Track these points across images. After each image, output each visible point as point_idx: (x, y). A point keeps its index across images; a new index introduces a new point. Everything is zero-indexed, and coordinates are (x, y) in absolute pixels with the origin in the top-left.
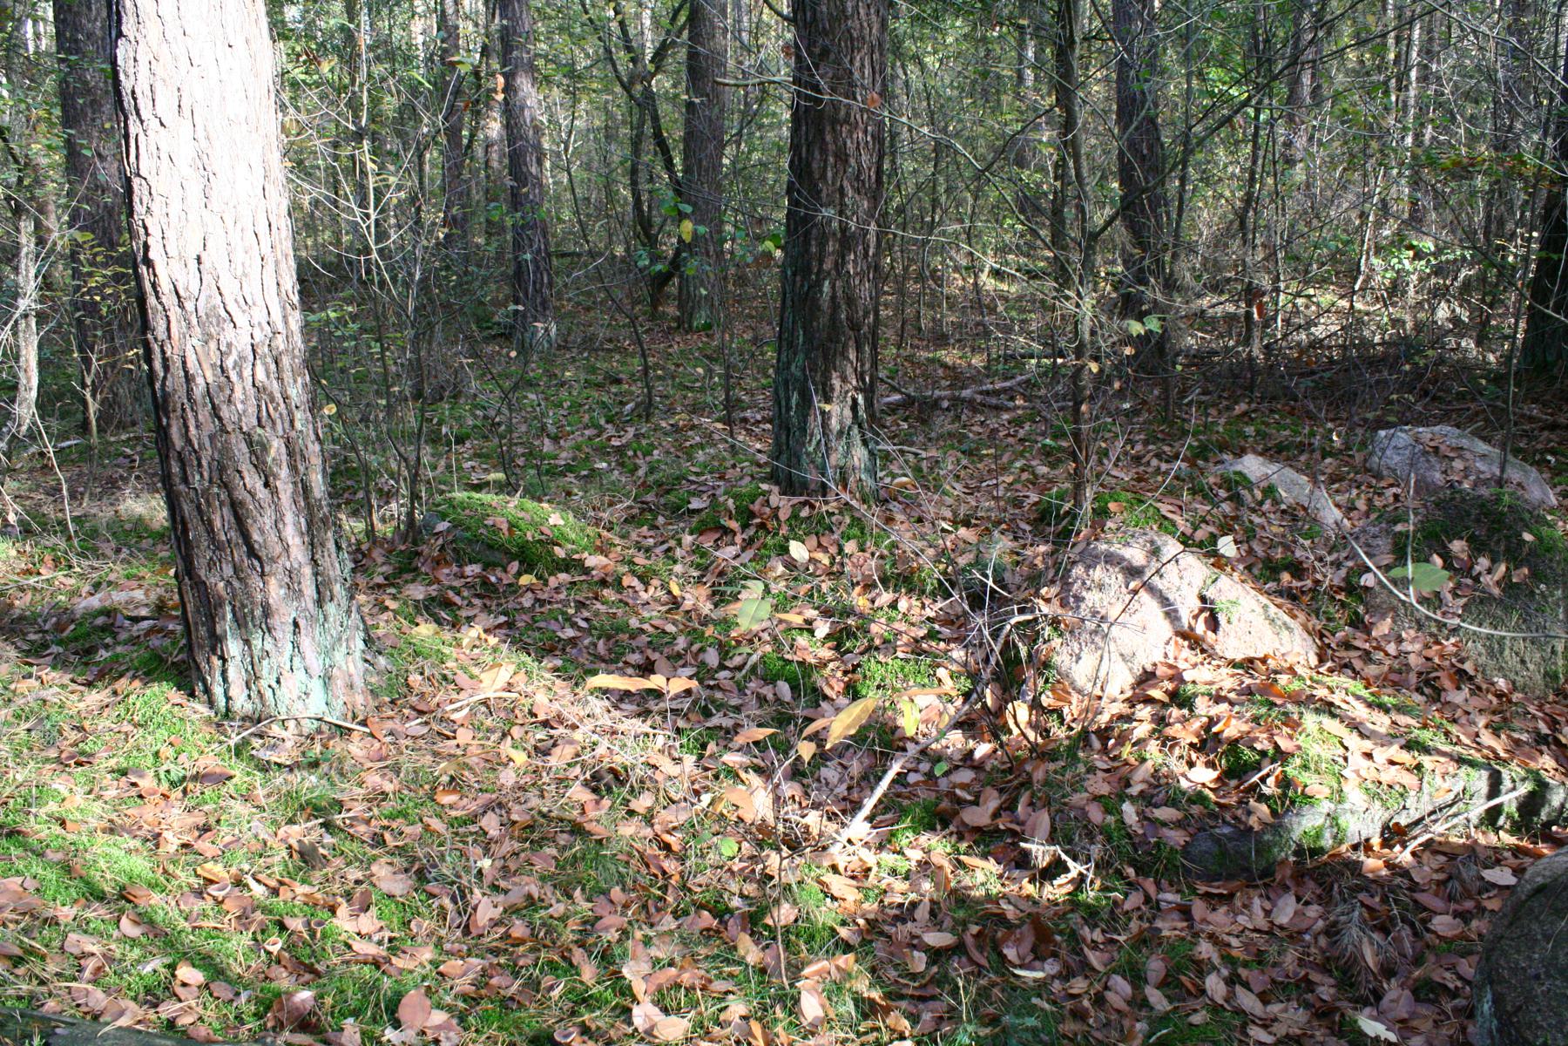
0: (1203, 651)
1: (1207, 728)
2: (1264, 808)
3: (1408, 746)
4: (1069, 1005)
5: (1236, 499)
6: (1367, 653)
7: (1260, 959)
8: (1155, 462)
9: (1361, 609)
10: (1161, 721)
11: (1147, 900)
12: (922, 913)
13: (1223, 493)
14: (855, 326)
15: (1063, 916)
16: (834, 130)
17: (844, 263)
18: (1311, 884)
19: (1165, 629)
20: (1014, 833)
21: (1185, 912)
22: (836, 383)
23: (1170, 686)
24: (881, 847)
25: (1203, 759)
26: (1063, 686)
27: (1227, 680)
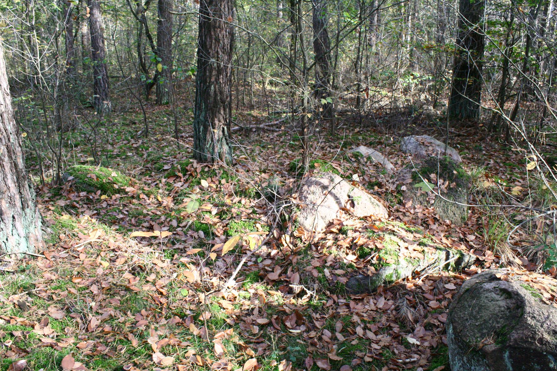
0: (349, 214)
1: (352, 241)
2: (373, 268)
3: (420, 244)
6: (404, 213)
7: (374, 320)
8: (329, 149)
9: (402, 198)
10: (336, 239)
11: (334, 302)
12: (256, 312)
13: (353, 159)
14: (223, 102)
16: (214, 30)
17: (219, 79)
19: (337, 207)
20: (287, 281)
21: (347, 306)
22: (217, 122)
23: (339, 227)
24: (239, 289)
25: (351, 252)
26: (301, 228)
27: (358, 224)
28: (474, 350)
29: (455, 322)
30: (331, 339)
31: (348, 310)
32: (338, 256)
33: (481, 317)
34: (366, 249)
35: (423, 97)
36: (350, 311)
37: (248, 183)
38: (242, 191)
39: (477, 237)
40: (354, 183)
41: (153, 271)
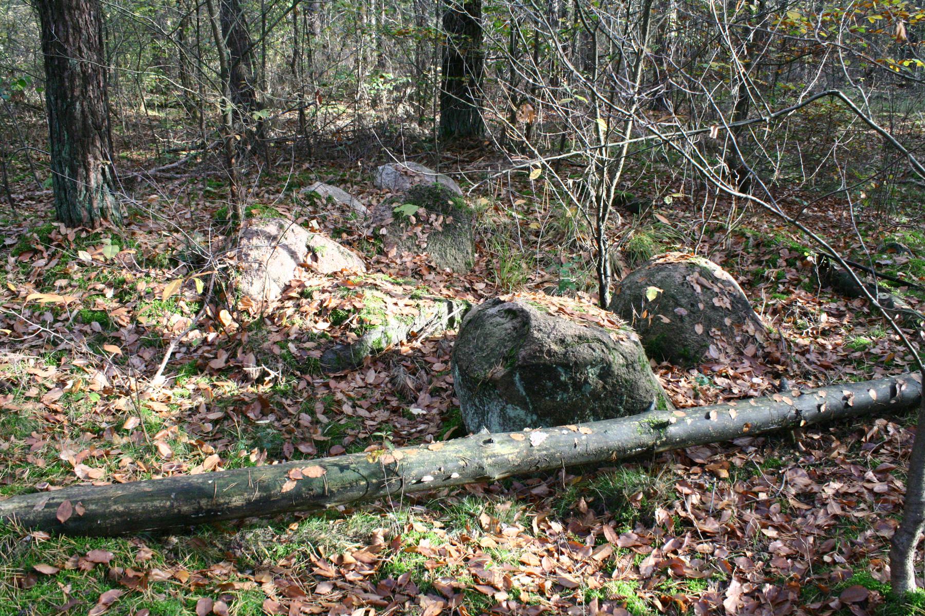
0: (312, 271)
1: (321, 305)
2: (353, 334)
3: (412, 298)
4: (284, 429)
5: (314, 204)
6: (388, 264)
7: (364, 396)
8: (266, 195)
9: (382, 246)
10: (298, 306)
11: (309, 384)
12: (203, 409)
13: (307, 203)
14: (98, 128)
15: (271, 396)
16: (70, 13)
17: (87, 92)
18: (380, 364)
19: (292, 264)
20: (238, 367)
21: (327, 386)
22: (91, 160)
23: (299, 290)
24: (172, 387)
25: (321, 319)
26: (247, 298)
27: (326, 283)
28: (483, 383)
30: (312, 423)
32: (304, 326)
33: (487, 346)
35: (400, 110)
37: (154, 248)
38: (147, 259)
39: (487, 284)
40: (313, 230)
41: (32, 383)
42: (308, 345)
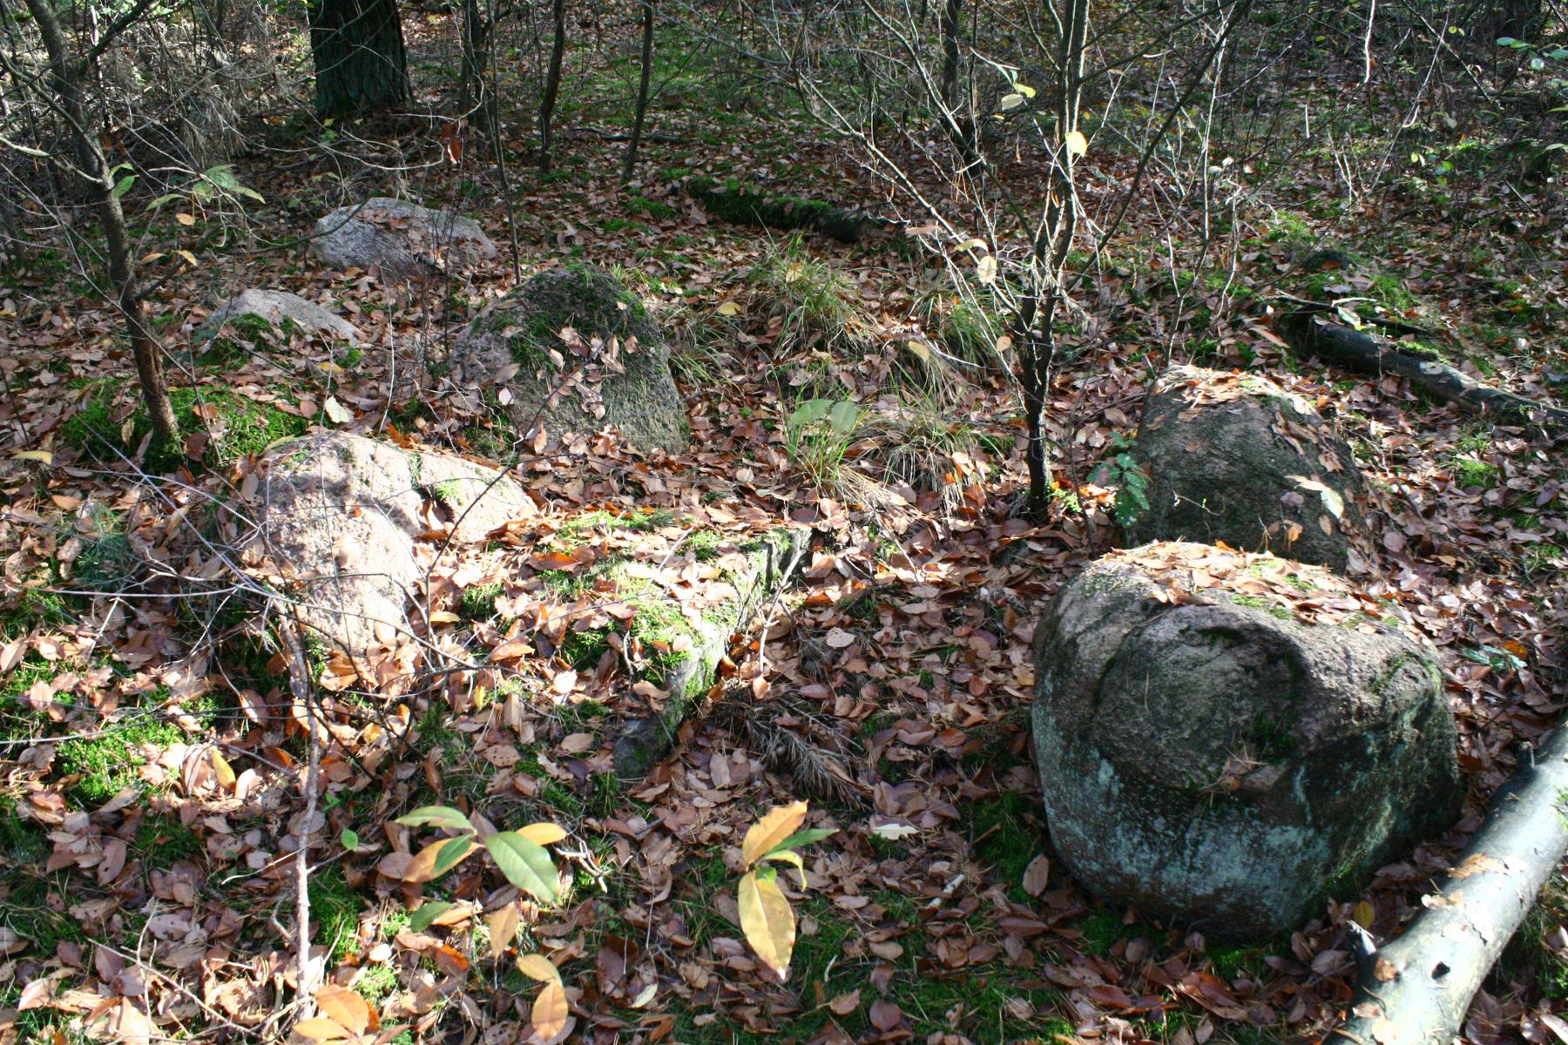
9: (512, 430)
19: (403, 540)
29: (1120, 752)
31: (668, 840)
33: (1187, 715)
34: (587, 635)
36: (675, 839)
42: (574, 743)
